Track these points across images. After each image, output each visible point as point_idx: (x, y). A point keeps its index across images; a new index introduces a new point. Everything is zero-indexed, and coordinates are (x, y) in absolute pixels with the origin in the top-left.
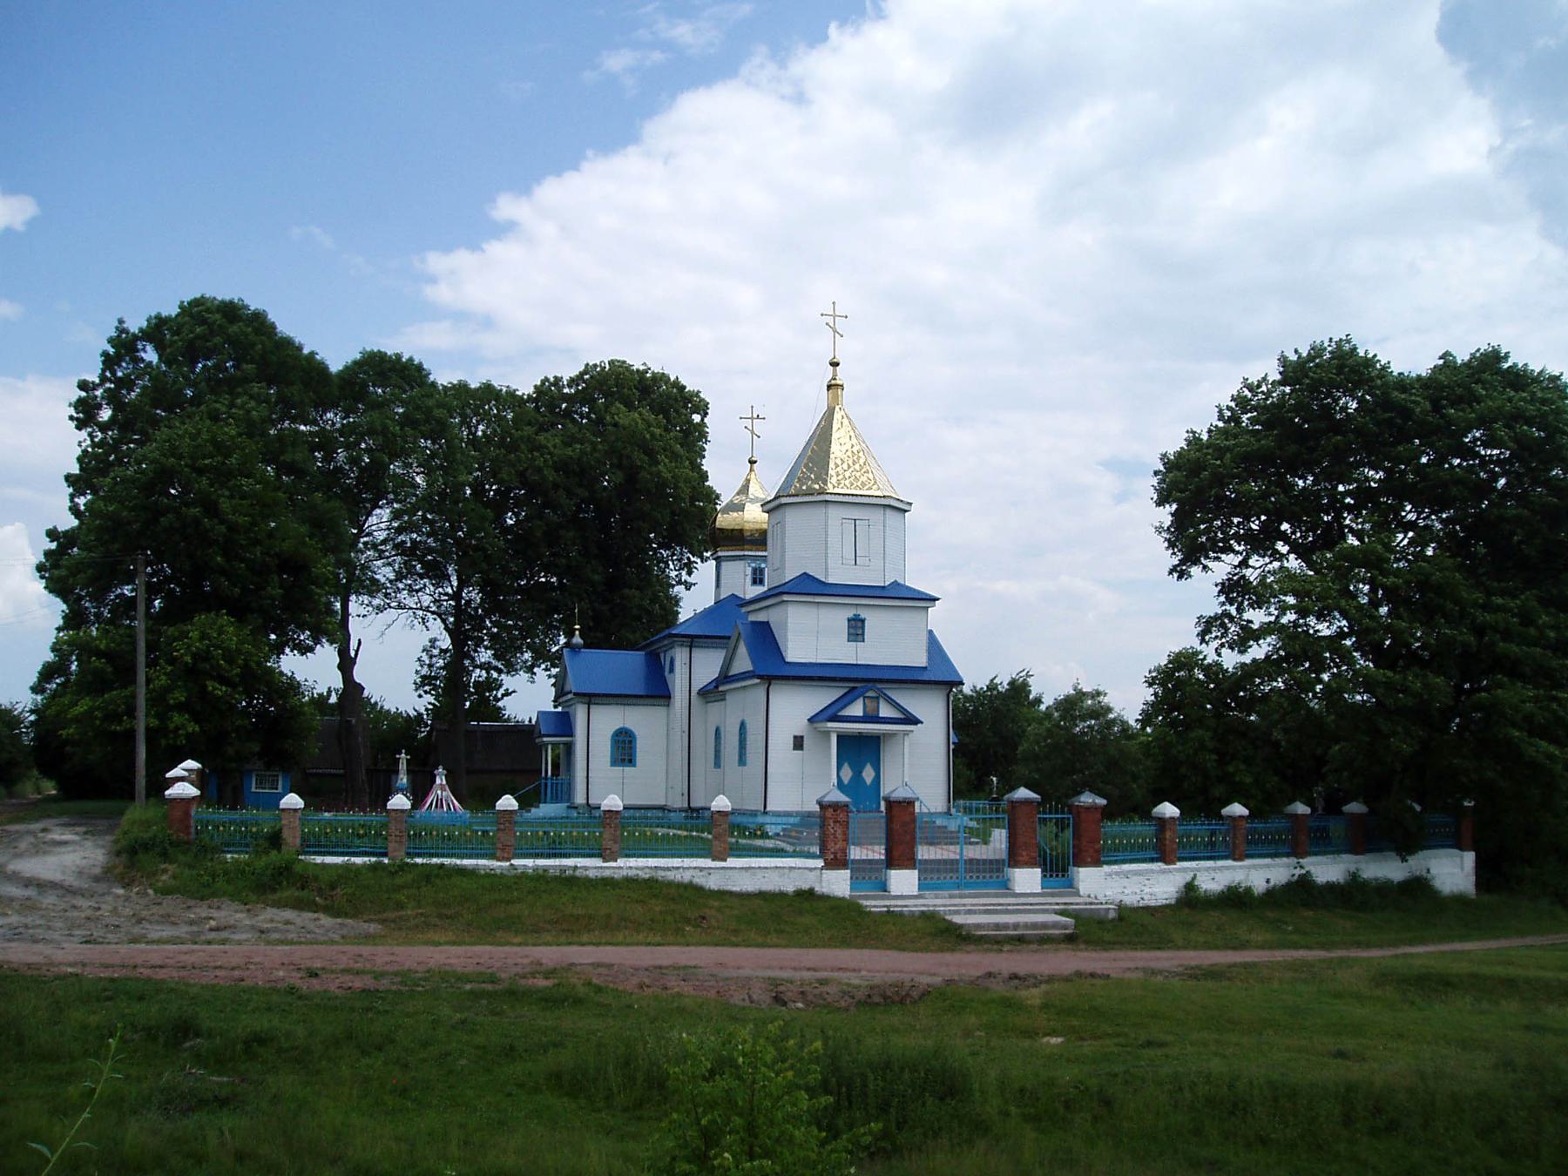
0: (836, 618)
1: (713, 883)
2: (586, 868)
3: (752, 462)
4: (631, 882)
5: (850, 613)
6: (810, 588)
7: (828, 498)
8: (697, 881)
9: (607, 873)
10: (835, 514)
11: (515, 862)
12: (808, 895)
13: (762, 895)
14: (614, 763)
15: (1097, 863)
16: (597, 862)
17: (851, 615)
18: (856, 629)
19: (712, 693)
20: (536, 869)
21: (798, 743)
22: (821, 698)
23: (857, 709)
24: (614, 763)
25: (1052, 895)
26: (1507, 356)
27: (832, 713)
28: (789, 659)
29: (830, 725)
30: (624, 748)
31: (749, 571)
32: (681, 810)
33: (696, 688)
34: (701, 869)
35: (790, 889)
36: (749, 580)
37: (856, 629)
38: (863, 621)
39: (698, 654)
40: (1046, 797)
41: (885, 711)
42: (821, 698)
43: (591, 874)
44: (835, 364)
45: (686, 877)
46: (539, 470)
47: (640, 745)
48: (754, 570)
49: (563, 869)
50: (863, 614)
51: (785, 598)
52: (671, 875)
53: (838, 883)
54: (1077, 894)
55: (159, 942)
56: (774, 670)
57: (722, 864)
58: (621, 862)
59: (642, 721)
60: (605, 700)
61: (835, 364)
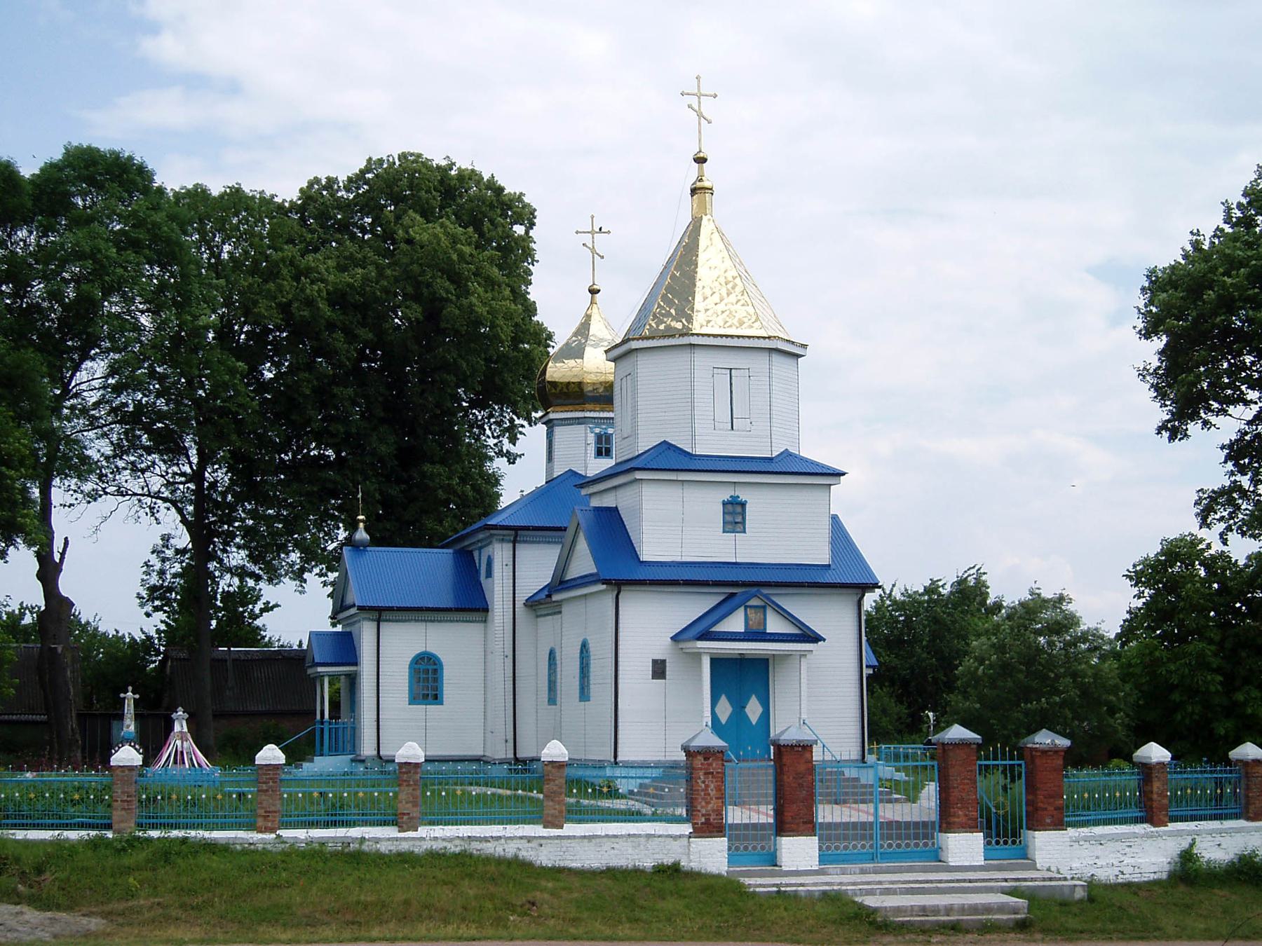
0: (706, 502)
1: (545, 857)
5: (726, 494)
6: (671, 461)
7: (694, 340)
9: (405, 846)
12: (672, 872)
13: (611, 873)
15: (1059, 825)
16: (390, 832)
17: (726, 497)
18: (735, 516)
19: (542, 604)
20: (309, 842)
21: (659, 669)
22: (687, 609)
23: (736, 623)
25: (999, 868)
27: (703, 630)
29: (700, 644)
30: (427, 680)
31: (591, 439)
33: (522, 597)
34: (529, 839)
35: (648, 863)
36: (592, 450)
37: (735, 516)
38: (743, 505)
39: (524, 552)
40: (989, 738)
41: (775, 625)
42: (687, 609)
43: (384, 848)
45: (510, 850)
48: (599, 438)
49: (346, 842)
50: (743, 495)
51: (639, 475)
52: (489, 848)
53: (711, 856)
54: (1033, 867)
56: (624, 571)
58: (423, 831)
59: (450, 642)
61: (701, 160)
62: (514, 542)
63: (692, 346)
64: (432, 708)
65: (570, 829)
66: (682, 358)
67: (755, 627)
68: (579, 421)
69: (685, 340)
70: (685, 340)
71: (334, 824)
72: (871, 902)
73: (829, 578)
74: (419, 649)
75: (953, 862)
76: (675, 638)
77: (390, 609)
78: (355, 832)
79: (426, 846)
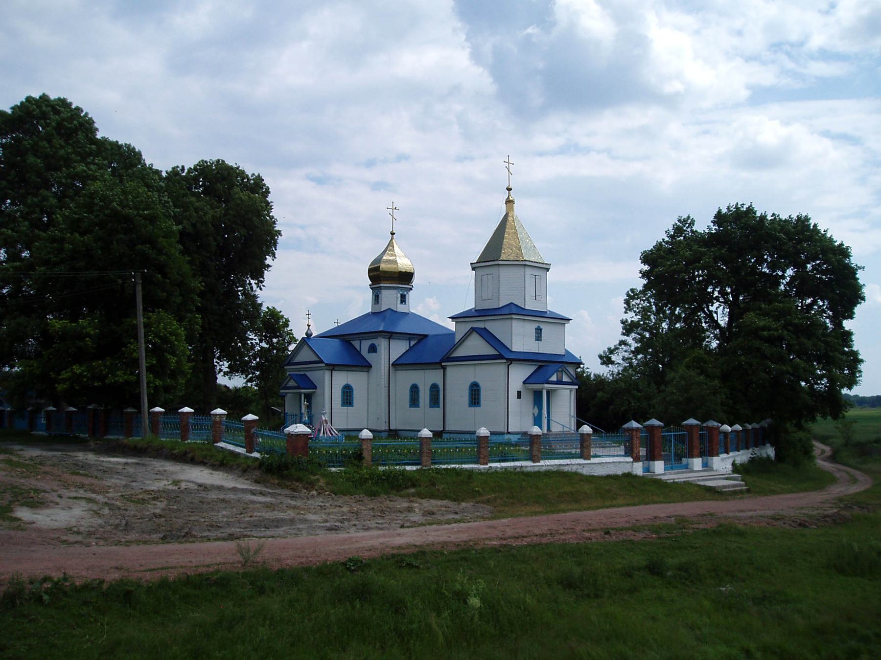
1: (585, 471)
2: (526, 467)
3: (393, 234)
4: (548, 474)
7: (501, 263)
8: (580, 471)
9: (536, 469)
10: (529, 272)
11: (490, 465)
12: (628, 476)
13: (608, 477)
14: (411, 406)
16: (529, 463)
20: (502, 468)
24: (411, 406)
26: (183, 169)
28: (513, 350)
31: (399, 296)
32: (385, 431)
34: (580, 465)
35: (620, 473)
38: (541, 330)
39: (393, 343)
40: (667, 424)
43: (529, 469)
44: (509, 189)
45: (574, 468)
46: (205, 223)
47: (356, 394)
48: (401, 295)
49: (515, 468)
51: (513, 316)
52: (566, 469)
54: (712, 470)
55: (448, 522)
57: (589, 462)
58: (542, 463)
59: (356, 379)
60: (343, 368)
61: (509, 189)
62: (389, 339)
63: (525, 265)
64: (350, 408)
65: (593, 460)
66: (521, 269)
67: (560, 379)
68: (394, 288)
69: (496, 262)
70: (496, 262)
71: (504, 461)
72: (702, 483)
73: (564, 360)
74: (344, 383)
75: (695, 469)
76: (524, 383)
77: (337, 365)
78: (518, 464)
79: (544, 468)
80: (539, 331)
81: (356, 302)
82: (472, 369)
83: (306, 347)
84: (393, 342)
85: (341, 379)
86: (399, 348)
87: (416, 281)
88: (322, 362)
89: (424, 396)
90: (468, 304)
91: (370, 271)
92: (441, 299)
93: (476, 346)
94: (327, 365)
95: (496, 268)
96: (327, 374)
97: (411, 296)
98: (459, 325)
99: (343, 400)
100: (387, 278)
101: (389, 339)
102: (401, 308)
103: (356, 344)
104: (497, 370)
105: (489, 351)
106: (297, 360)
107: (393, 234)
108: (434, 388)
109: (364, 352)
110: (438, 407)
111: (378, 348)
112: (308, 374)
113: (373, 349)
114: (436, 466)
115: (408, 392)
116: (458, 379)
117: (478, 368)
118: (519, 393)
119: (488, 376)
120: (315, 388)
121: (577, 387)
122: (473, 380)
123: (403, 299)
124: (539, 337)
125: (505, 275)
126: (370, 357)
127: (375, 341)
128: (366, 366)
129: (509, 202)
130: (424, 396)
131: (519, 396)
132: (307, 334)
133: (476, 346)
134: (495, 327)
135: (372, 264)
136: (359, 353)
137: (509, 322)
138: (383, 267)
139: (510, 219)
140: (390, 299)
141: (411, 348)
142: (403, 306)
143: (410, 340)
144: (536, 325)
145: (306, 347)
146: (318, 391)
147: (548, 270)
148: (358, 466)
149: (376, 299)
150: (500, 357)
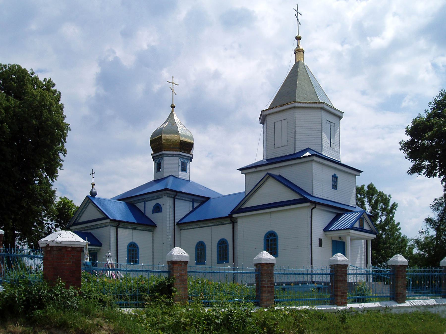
3: (173, 107)
7: (297, 105)
31: (180, 164)
48: (135, 262)
59: (141, 238)
62: (174, 198)
77: (123, 222)
80: (335, 178)
81: (139, 171)
82: (267, 217)
83: (90, 205)
84: (177, 202)
85: (126, 236)
86: (183, 209)
87: (195, 151)
88: (107, 218)
89: (212, 253)
90: (259, 156)
91: (152, 142)
92: (221, 164)
93: (273, 192)
94: (112, 220)
95: (291, 112)
96: (112, 230)
97: (192, 166)
98: (249, 176)
99: (129, 257)
100: (169, 147)
101: (174, 198)
102: (182, 175)
103: (140, 206)
104: (301, 213)
105: (291, 196)
106: (82, 219)
107: (173, 107)
108: (222, 246)
109: (149, 213)
110: (227, 262)
111: (163, 207)
112: (92, 232)
113: (158, 209)
114: (359, 253)
115: (194, 250)
116: (251, 229)
117: (274, 216)
118: (320, 240)
119: (284, 223)
120: (100, 245)
121: (375, 236)
122: (269, 229)
123: (184, 168)
124: (335, 186)
125: (302, 119)
126: (155, 217)
127: (159, 201)
128: (150, 226)
129: (298, 51)
130: (212, 253)
131: (320, 245)
132: (91, 193)
133: (273, 192)
134: (290, 172)
135: (152, 136)
136: (143, 214)
137: (309, 165)
138: (165, 136)
139: (300, 67)
140: (171, 164)
141: (194, 209)
142: (184, 173)
143: (193, 201)
144: (332, 172)
145: (90, 205)
146: (103, 248)
147: (340, 118)
148: (168, 304)
149: (158, 167)
150: (304, 200)
